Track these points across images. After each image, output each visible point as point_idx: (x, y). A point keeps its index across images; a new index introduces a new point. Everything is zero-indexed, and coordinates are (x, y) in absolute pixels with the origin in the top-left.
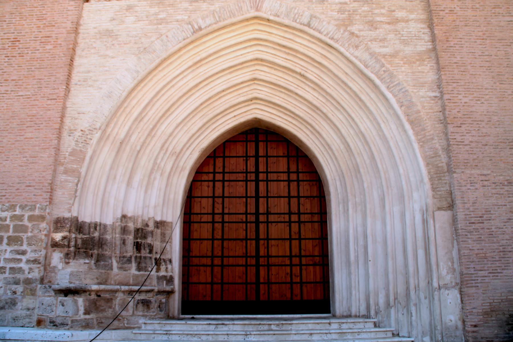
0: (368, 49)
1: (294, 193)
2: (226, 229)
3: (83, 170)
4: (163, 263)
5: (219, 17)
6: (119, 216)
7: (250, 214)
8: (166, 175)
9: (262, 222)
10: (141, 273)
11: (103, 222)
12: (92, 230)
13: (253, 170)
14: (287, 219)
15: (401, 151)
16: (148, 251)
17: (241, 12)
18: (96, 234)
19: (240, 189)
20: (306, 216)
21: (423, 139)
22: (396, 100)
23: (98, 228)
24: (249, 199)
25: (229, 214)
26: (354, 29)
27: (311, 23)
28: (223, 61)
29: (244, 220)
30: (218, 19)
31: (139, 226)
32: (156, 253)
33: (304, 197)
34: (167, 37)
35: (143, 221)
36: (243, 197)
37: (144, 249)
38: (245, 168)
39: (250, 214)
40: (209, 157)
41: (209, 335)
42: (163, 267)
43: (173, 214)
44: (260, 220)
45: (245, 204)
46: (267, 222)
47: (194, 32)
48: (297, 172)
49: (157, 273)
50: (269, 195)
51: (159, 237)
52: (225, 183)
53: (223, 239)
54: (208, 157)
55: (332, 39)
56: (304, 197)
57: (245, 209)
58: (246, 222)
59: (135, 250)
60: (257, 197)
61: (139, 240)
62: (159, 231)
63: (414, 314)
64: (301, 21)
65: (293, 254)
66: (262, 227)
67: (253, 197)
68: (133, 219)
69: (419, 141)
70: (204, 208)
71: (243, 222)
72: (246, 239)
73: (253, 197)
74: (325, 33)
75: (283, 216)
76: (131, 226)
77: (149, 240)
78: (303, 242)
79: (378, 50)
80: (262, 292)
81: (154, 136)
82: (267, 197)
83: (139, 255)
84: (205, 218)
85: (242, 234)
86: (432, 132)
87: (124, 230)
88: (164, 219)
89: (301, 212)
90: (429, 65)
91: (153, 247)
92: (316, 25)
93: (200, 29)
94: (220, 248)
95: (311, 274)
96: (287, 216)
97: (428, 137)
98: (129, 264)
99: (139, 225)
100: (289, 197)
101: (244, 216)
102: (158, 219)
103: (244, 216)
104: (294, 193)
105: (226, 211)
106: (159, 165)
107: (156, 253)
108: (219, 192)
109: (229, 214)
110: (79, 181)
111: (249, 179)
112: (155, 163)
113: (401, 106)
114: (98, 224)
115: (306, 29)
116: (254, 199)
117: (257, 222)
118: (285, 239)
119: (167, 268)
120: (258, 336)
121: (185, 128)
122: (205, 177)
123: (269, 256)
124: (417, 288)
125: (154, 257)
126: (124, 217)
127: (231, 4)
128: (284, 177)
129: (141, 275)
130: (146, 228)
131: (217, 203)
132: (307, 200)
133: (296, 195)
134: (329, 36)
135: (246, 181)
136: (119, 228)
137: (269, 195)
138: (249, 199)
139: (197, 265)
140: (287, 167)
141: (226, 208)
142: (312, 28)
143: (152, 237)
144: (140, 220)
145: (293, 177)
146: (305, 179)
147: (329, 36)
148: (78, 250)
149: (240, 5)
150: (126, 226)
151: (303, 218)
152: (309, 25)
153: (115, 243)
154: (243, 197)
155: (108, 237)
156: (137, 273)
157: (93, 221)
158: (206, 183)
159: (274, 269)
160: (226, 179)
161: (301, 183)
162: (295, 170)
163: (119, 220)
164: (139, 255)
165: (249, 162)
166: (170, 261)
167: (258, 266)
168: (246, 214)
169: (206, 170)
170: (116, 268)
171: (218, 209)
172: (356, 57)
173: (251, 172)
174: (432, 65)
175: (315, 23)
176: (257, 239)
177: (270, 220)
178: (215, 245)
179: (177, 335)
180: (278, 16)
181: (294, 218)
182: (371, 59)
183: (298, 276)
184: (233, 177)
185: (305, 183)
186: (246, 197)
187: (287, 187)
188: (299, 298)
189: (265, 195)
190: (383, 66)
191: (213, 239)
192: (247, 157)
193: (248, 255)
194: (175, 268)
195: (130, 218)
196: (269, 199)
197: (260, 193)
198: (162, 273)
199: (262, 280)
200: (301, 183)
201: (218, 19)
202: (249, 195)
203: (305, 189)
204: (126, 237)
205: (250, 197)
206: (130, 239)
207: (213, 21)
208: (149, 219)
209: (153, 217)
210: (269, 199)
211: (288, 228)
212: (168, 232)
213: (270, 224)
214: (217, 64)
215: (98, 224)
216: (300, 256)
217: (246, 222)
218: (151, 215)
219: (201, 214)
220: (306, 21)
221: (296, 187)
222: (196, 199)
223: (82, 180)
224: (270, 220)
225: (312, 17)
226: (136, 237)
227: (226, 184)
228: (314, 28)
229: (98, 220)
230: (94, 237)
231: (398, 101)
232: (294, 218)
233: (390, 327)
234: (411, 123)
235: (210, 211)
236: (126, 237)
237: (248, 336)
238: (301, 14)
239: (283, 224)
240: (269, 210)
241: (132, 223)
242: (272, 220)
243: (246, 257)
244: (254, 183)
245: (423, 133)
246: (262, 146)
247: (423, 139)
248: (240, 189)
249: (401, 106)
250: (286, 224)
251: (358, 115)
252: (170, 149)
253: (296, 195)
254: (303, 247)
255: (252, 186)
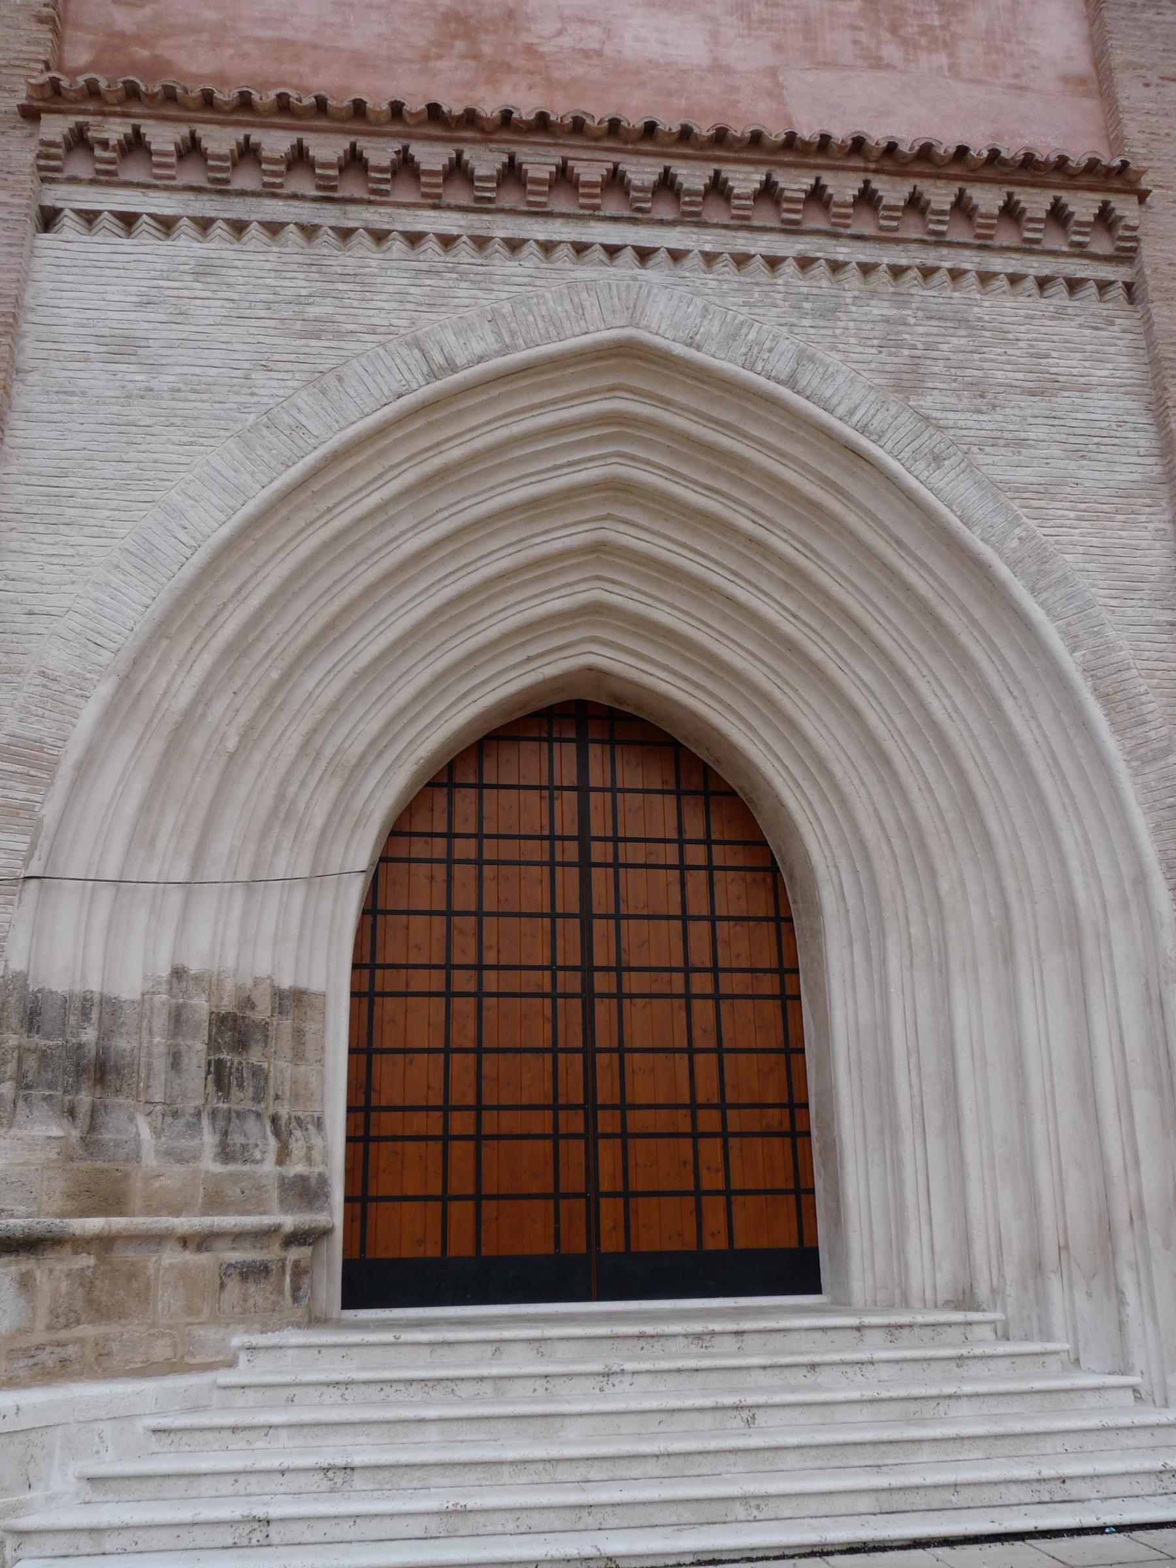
0: (972, 467)
1: (698, 906)
2: (489, 1016)
3: (49, 812)
4: (298, 1133)
5: (513, 334)
6: (165, 972)
7: (565, 968)
8: (312, 836)
9: (603, 996)
10: (232, 1167)
11: (113, 991)
12: (72, 1020)
13: (572, 830)
14: (679, 988)
15: (1067, 786)
16: (250, 1092)
17: (582, 323)
18: (89, 1036)
19: (532, 890)
20: (737, 976)
21: (1142, 751)
22: (1058, 627)
23: (94, 1015)
24: (559, 921)
25: (497, 968)
26: (927, 403)
27: (799, 376)
28: (512, 481)
29: (548, 988)
30: (508, 340)
31: (228, 1005)
32: (277, 1097)
33: (728, 919)
34: (340, 379)
35: (239, 988)
36: (542, 915)
37: (241, 1086)
38: (546, 821)
39: (565, 968)
40: (432, 784)
41: (482, 1379)
42: (297, 1146)
43: (327, 970)
44: (598, 989)
45: (548, 937)
46: (620, 996)
47: (433, 375)
48: (708, 842)
49: (278, 1168)
50: (623, 911)
51: (285, 1042)
52: (486, 868)
53: (479, 1051)
54: (427, 785)
55: (863, 430)
56: (728, 919)
57: (548, 953)
58: (554, 996)
59: (211, 1088)
60: (586, 917)
61: (225, 1056)
62: (287, 1023)
63: (1131, 1295)
64: (768, 367)
65: (701, 1099)
66: (603, 1010)
67: (573, 916)
68: (208, 983)
69: (1130, 755)
70: (418, 947)
71: (543, 995)
72: (554, 1050)
73: (573, 916)
74: (841, 410)
75: (665, 975)
76: (201, 1006)
77: (255, 1056)
78: (728, 1058)
79: (999, 474)
80: (606, 1223)
81: (280, 708)
82: (618, 917)
83: (226, 1106)
84: (421, 981)
85: (541, 1036)
86: (1164, 731)
87: (178, 1018)
88: (303, 984)
89: (721, 964)
90: (1151, 526)
91: (266, 1079)
92: (815, 383)
93: (453, 368)
94: (471, 1078)
95: (756, 1164)
96: (679, 978)
97: (1156, 746)
98: (192, 1137)
99: (225, 1002)
100: (685, 918)
101: (547, 974)
102: (286, 983)
103: (547, 974)
104: (698, 906)
105: (490, 958)
106: (293, 802)
107: (277, 1097)
108: (464, 898)
109: (497, 968)
110: (33, 846)
111: (558, 858)
112: (280, 797)
113: (1073, 650)
114: (96, 998)
115: (785, 392)
116: (577, 921)
117: (588, 997)
118: (675, 1051)
119: (310, 1148)
120: (672, 1381)
121: (378, 689)
122: (419, 848)
123: (623, 1107)
124: (1138, 1213)
125: (271, 1111)
126: (178, 973)
127: (549, 295)
128: (670, 854)
129: (231, 1174)
130: (248, 1013)
131: (462, 932)
132: (738, 928)
133: (705, 912)
134: (855, 418)
135: (552, 864)
136: (165, 1011)
137: (623, 911)
138: (559, 921)
139: (395, 1138)
140: (675, 823)
141: (490, 948)
142: (798, 393)
143: (266, 1043)
144: (229, 987)
145: (696, 855)
146: (730, 863)
147: (855, 418)
148: (22, 1092)
149: (576, 300)
150: (184, 1005)
151: (728, 984)
152: (791, 382)
153: (149, 1066)
154: (542, 915)
155: (122, 1043)
156: (217, 1168)
157: (77, 988)
158: (425, 867)
159: (640, 1150)
160: (486, 856)
161: (718, 875)
162: (700, 835)
163: (164, 987)
164: (226, 1106)
165: (557, 804)
166: (319, 1124)
167: (591, 1137)
168: (553, 968)
169: (420, 825)
170: (152, 1154)
171: (463, 952)
172: (937, 493)
173: (564, 838)
174: (1161, 526)
175: (809, 378)
176: (589, 1050)
177: (625, 990)
178: (454, 1071)
179: (372, 1387)
180: (699, 348)
181: (701, 983)
182: (980, 498)
183: (718, 1171)
184: (508, 850)
185: (731, 874)
186: (553, 916)
187: (676, 889)
188: (721, 1244)
189: (612, 911)
190: (1016, 521)
191: (448, 1051)
192: (551, 789)
193: (562, 1101)
194: (330, 1151)
195: (197, 979)
196: (623, 923)
197: (595, 904)
198: (297, 1168)
199: (605, 1186)
200: (718, 875)
201: (508, 340)
202: (559, 910)
203: (734, 894)
204: (183, 1043)
205: (565, 916)
206: (196, 1050)
207: (491, 343)
208: (257, 982)
209: (269, 977)
210: (623, 923)
211: (684, 1014)
212: (311, 1027)
213: (626, 1002)
214: (493, 488)
215: (96, 998)
216: (723, 1107)
217: (554, 996)
218: (263, 968)
219: (408, 967)
220: (783, 368)
221: (704, 889)
222: (390, 918)
223: (44, 843)
224: (625, 990)
225: (803, 357)
226: (213, 1045)
227: (488, 871)
228: (808, 393)
229: (94, 985)
230: (80, 1046)
231: (1064, 634)
232: (701, 983)
233: (1048, 1337)
234: (1105, 698)
235: (438, 958)
236: (183, 1043)
237: (612, 1379)
238: (768, 345)
239: (666, 1002)
240: (624, 957)
241: (204, 997)
242: (634, 991)
243: (555, 1108)
244: (576, 870)
245: (1139, 730)
246: (599, 757)
247: (1142, 751)
248: (532, 890)
249: (1073, 650)
250: (676, 1001)
251: (925, 672)
252: (329, 751)
253: (705, 912)
254: (486, 1070)
255: (569, 879)
